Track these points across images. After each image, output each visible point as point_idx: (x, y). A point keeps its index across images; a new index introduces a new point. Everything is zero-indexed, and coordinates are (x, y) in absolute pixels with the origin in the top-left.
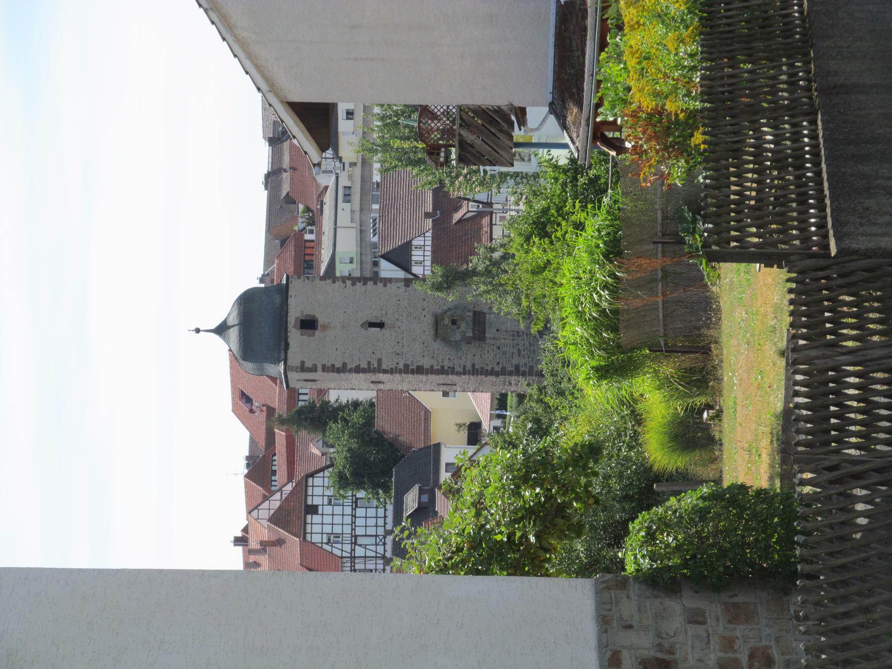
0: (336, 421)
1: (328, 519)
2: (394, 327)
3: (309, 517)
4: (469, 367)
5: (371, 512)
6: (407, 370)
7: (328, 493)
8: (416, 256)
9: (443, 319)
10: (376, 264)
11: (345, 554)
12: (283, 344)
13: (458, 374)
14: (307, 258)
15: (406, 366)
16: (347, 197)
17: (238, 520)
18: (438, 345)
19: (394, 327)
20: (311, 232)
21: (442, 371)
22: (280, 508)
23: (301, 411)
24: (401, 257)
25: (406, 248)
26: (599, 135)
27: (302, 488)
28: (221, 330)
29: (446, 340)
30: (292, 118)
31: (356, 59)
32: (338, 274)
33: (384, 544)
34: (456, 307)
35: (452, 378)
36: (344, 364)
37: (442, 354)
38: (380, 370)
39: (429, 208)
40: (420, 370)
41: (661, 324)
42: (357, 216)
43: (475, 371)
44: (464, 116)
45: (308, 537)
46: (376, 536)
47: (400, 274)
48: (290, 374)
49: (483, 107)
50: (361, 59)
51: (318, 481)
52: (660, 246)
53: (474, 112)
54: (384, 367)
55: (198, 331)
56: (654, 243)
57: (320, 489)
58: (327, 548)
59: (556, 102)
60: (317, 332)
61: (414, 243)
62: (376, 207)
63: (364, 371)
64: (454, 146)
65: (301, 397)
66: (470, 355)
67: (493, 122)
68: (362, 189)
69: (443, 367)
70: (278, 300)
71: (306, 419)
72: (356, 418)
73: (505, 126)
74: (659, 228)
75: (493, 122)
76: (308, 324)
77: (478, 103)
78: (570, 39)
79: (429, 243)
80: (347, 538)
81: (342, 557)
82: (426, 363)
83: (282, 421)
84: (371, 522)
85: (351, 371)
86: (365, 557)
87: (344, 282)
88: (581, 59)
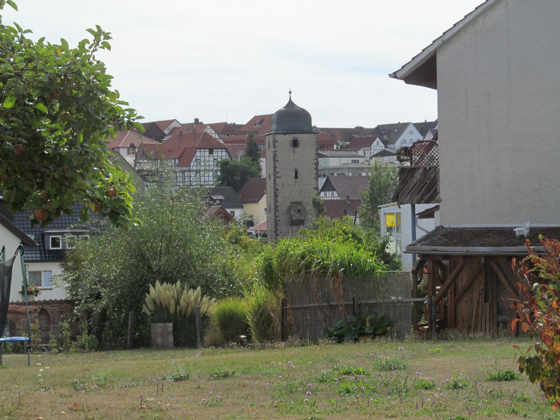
0: (252, 160)
1: (207, 158)
2: (296, 183)
3: (208, 150)
4: (278, 219)
5: (211, 179)
6: (276, 190)
7: (219, 158)
8: (329, 194)
9: (300, 206)
10: (324, 176)
11: (191, 167)
12: (286, 132)
13: (275, 214)
14: (325, 146)
15: (278, 190)
16: (354, 162)
17: (205, 120)
18: (288, 204)
19: (296, 183)
20: (337, 148)
21: (276, 206)
22: (211, 137)
23: (255, 144)
24: (328, 186)
25: (333, 189)
26: (425, 259)
27: (221, 147)
28: (291, 103)
29: (290, 208)
30: (424, 58)
31: (467, 97)
32: (319, 159)
33: (196, 185)
34: (306, 212)
35: (273, 211)
36: (277, 161)
37: (284, 206)
38: (275, 178)
39: (352, 198)
40: (276, 196)
41: (301, 306)
42: (346, 166)
43: (276, 222)
44: (431, 170)
45: (198, 150)
46: (200, 181)
47: (320, 188)
48: (272, 136)
49: (438, 183)
50: (467, 101)
51: (224, 154)
52: (352, 303)
53: (435, 177)
54: (277, 179)
55: (290, 92)
56: (354, 299)
57: (221, 155)
58: (194, 159)
59: (444, 230)
60: (292, 148)
61: (335, 192)
62: (350, 174)
63: (275, 170)
64: (411, 164)
65: (262, 146)
66: (283, 219)
67: (429, 189)
68: (359, 168)
69: (278, 207)
70: (306, 129)
71: (252, 147)
72: (253, 169)
73: (426, 198)
74: (364, 302)
75: (429, 189)
76: (295, 144)
77: (440, 179)
78: (488, 237)
79: (335, 199)
80: (198, 168)
81: (190, 166)
82: (280, 199)
83: (251, 136)
84: (207, 179)
85: (274, 164)
86: (190, 177)
87: (315, 159)
88: (477, 244)
